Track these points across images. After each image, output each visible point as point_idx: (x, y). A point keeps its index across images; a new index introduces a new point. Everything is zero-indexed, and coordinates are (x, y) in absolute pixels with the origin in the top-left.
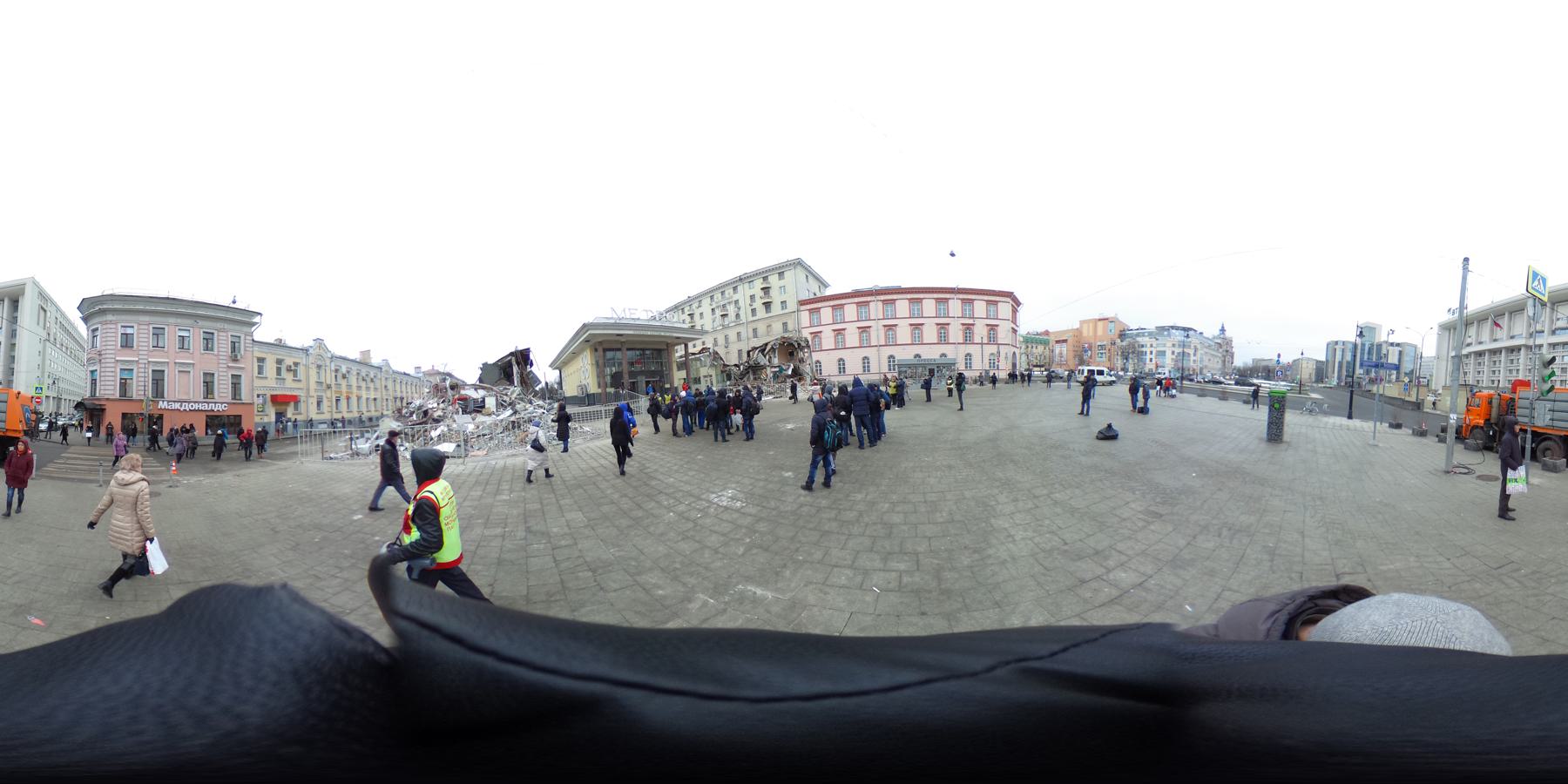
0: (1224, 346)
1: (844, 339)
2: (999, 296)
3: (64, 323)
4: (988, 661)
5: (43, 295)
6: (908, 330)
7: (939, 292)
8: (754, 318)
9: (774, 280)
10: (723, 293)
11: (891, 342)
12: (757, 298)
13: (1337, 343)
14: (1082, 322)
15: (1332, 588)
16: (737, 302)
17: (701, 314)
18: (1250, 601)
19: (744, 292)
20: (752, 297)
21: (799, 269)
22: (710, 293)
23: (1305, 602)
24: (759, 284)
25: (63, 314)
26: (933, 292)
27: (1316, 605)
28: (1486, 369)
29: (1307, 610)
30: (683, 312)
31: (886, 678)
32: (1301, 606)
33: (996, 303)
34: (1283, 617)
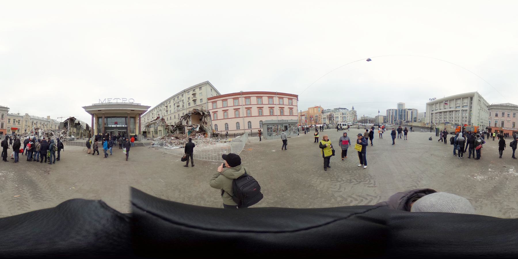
0: (354, 113)
1: (217, 115)
2: (293, 96)
3: (485, 104)
4: (349, 214)
5: (480, 97)
6: (268, 109)
7: (280, 95)
8: (189, 107)
9: (197, 91)
10: (178, 97)
11: (261, 114)
12: (191, 98)
13: (390, 110)
14: (309, 109)
15: (423, 190)
16: (183, 100)
17: (170, 106)
18: (398, 193)
19: (186, 96)
20: (189, 98)
21: (208, 85)
22: (173, 98)
23: (413, 194)
24: (191, 92)
25: (485, 101)
26: (267, 94)
27: (418, 195)
28: (448, 117)
29: (414, 196)
30: (164, 106)
31: (323, 221)
32: (411, 196)
33: (292, 99)
34: (405, 198)
